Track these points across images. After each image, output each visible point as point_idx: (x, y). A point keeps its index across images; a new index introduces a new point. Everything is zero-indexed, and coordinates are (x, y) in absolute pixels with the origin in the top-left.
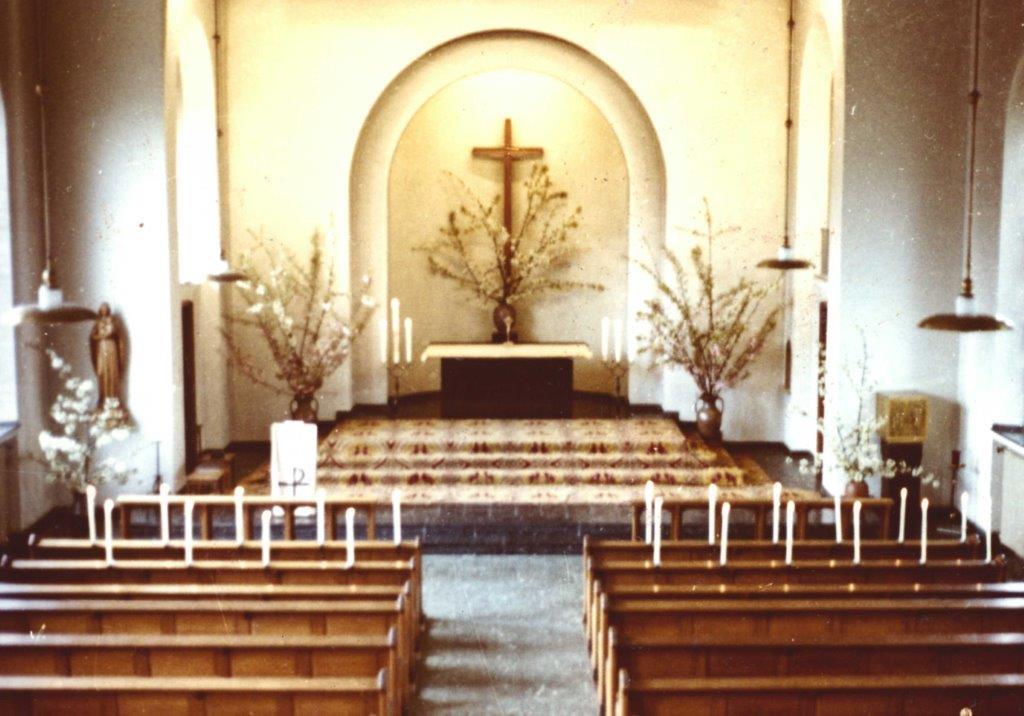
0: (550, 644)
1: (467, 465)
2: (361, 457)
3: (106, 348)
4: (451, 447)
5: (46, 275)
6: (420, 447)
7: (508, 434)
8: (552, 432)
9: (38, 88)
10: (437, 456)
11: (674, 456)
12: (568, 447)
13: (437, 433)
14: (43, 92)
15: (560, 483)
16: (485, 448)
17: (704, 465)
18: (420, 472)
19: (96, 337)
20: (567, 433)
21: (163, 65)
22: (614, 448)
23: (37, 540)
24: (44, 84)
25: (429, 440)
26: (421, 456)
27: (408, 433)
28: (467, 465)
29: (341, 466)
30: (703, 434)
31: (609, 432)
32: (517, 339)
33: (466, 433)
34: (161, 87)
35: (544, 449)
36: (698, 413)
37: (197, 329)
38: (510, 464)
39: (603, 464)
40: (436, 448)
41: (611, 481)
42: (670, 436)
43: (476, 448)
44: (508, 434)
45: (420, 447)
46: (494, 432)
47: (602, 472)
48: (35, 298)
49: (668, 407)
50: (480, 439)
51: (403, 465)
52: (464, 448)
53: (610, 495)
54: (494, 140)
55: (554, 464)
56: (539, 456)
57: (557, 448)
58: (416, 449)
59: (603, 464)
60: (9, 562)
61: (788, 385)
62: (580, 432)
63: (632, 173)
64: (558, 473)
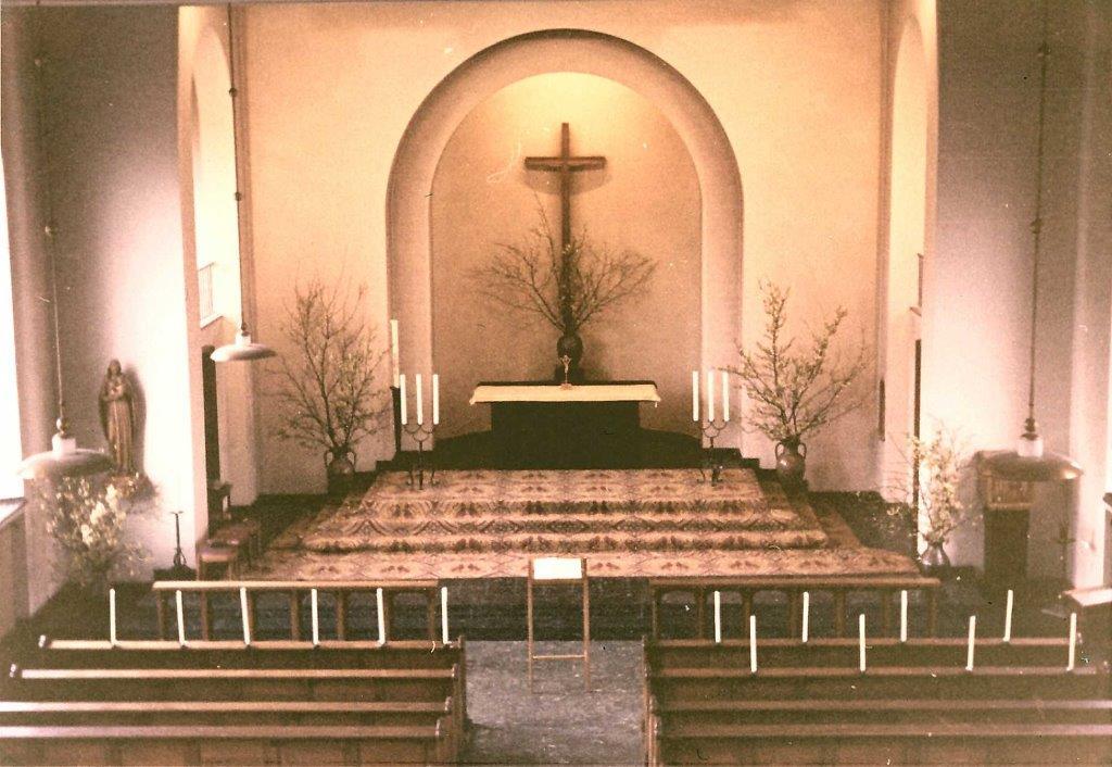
0: (942, 715)
1: (519, 528)
2: (402, 520)
3: (117, 409)
4: (501, 507)
5: (59, 423)
6: (468, 505)
7: (566, 490)
8: (614, 487)
9: (47, 230)
10: (487, 518)
11: (748, 517)
12: (632, 507)
13: (485, 489)
14: (52, 233)
15: (621, 549)
16: (539, 508)
17: (784, 526)
18: (467, 538)
19: (106, 399)
20: (631, 489)
21: (174, 85)
22: (683, 507)
23: (48, 642)
24: (52, 224)
25: (478, 499)
26: (468, 519)
27: (459, 489)
28: (519, 528)
29: (379, 530)
30: (786, 485)
31: (678, 486)
32: (579, 377)
33: (519, 488)
34: (174, 114)
35: (605, 508)
36: (778, 458)
37: (219, 388)
38: (566, 527)
39: (670, 526)
40: (484, 508)
41: (678, 546)
42: (746, 491)
43: (530, 508)
44: (566, 490)
45: (468, 505)
46: (551, 487)
47: (668, 536)
48: (49, 447)
49: (745, 454)
50: (535, 497)
51: (449, 529)
52: (516, 508)
53: (679, 565)
54: (548, 147)
55: (615, 527)
56: (599, 517)
57: (619, 508)
58: (463, 509)
59: (670, 526)
60: (18, 672)
61: (881, 430)
62: (647, 486)
63: (702, 183)
64: (620, 537)
